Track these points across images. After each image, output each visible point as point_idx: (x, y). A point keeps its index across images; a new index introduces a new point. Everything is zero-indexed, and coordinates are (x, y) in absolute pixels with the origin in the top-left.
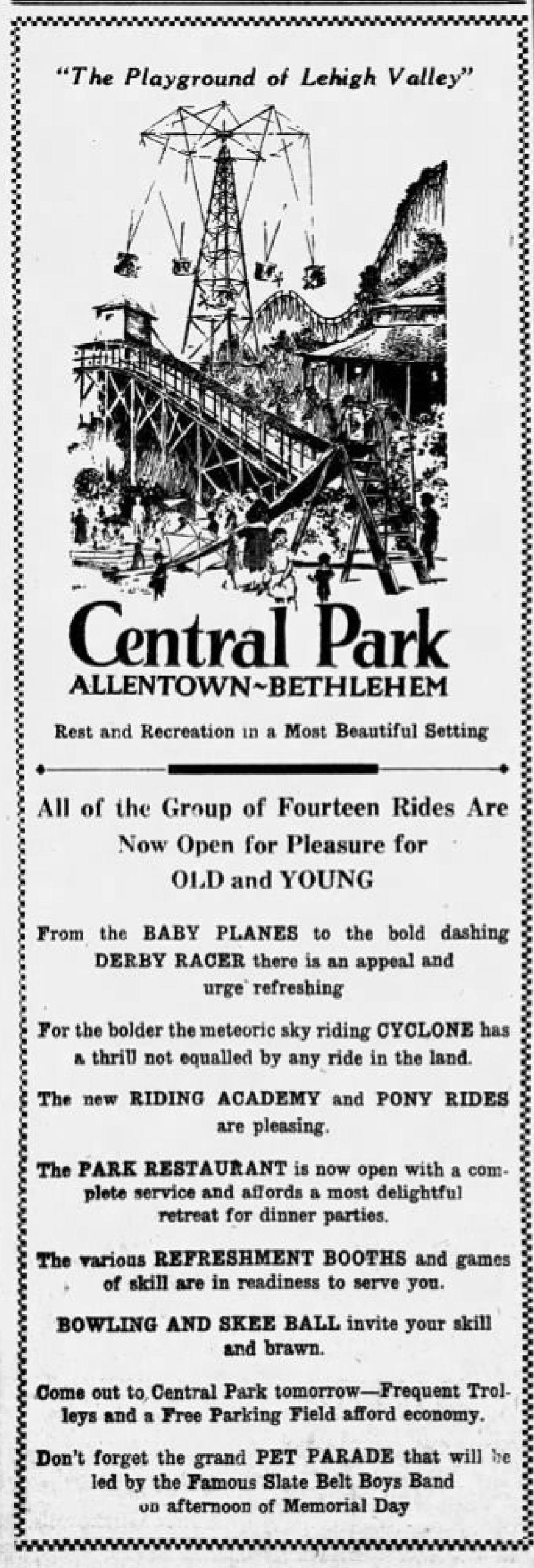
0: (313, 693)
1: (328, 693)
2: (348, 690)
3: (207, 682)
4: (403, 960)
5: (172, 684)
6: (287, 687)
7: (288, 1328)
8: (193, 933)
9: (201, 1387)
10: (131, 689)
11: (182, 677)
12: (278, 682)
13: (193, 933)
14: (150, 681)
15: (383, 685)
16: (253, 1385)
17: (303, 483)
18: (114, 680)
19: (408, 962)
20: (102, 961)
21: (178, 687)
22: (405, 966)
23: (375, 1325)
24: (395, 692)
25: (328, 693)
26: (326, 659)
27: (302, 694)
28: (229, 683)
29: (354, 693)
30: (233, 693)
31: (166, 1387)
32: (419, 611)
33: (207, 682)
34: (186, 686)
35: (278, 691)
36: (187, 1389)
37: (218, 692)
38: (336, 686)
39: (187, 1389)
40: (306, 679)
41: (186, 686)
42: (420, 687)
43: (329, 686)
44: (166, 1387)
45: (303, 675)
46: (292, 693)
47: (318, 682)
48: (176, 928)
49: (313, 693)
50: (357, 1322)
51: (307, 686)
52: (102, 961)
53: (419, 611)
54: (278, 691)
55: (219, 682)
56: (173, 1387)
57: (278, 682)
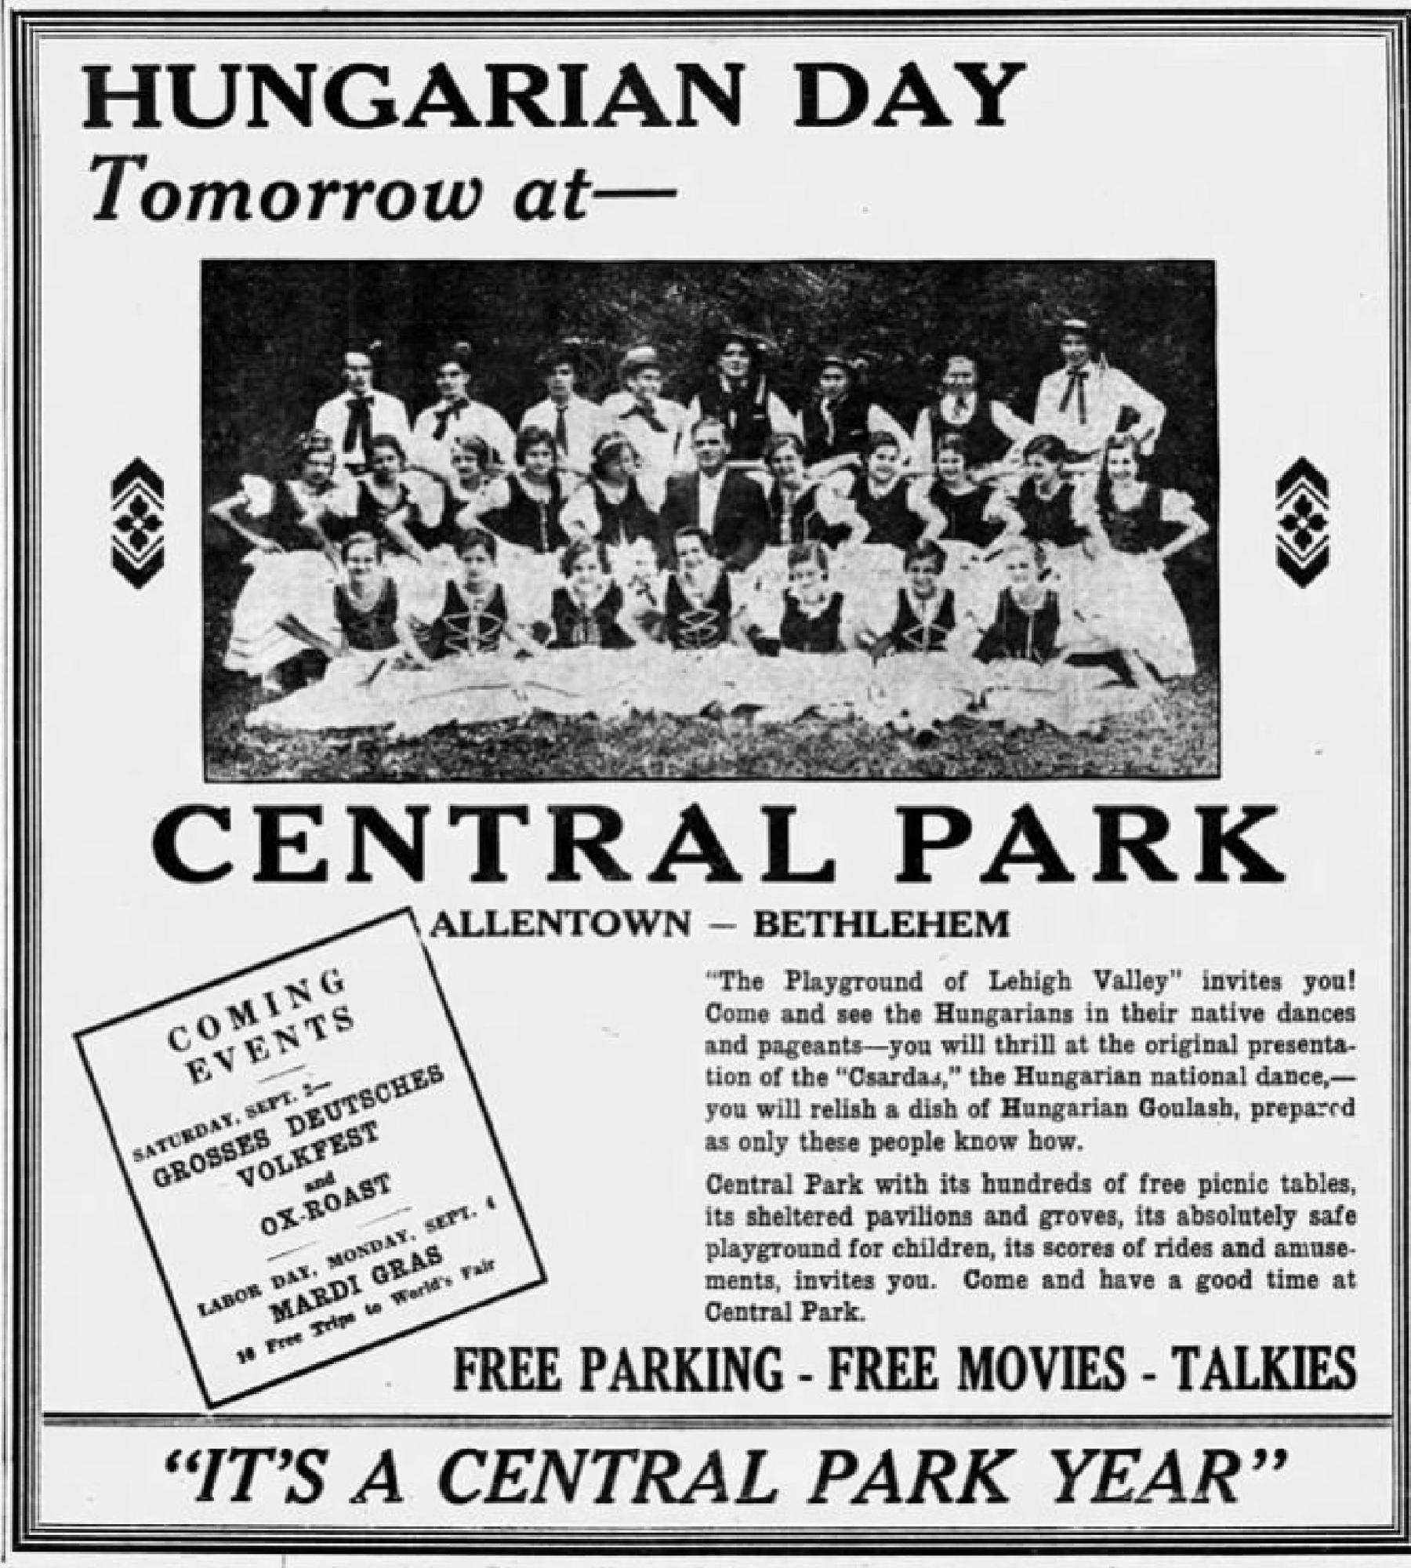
0: (819, 933)
1: (839, 933)
2: (865, 928)
3: (636, 917)
4: (1223, 1043)
5: (585, 922)
6: (780, 922)
7: (1006, 1114)
8: (990, 96)
9: (772, 1177)
10: (523, 928)
11: (599, 914)
12: (767, 918)
13: (990, 96)
14: (554, 917)
15: (914, 924)
16: (844, 1176)
17: (1138, 376)
18: (472, 919)
19: (1230, 1046)
20: (297, 1125)
21: (595, 925)
22: (1226, 1051)
23: (832, 1283)
24: (848, 930)
25: (839, 933)
26: (913, 872)
27: (802, 934)
28: (663, 918)
29: (871, 933)
30: (668, 933)
31: (725, 1177)
32: (210, 1499)
33: (636, 917)
34: (606, 923)
35: (767, 929)
36: (754, 1181)
37: (649, 929)
38: (931, 924)
39: (754, 1181)
40: (809, 914)
41: (606, 923)
42: (525, 923)
43: (840, 924)
44: (725, 1177)
45: (804, 909)
46: (787, 933)
47: (825, 918)
48: (649, 1351)
49: (819, 933)
50: (807, 1278)
51: (809, 924)
52: (297, 1125)
53: (210, 1499)
54: (767, 929)
55: (650, 917)
56: (734, 1177)
57: (767, 918)
